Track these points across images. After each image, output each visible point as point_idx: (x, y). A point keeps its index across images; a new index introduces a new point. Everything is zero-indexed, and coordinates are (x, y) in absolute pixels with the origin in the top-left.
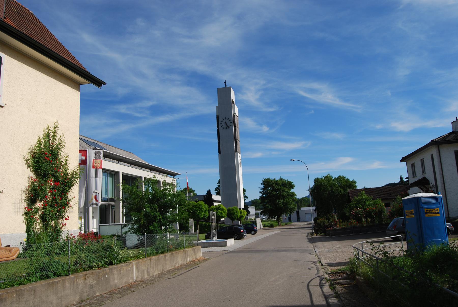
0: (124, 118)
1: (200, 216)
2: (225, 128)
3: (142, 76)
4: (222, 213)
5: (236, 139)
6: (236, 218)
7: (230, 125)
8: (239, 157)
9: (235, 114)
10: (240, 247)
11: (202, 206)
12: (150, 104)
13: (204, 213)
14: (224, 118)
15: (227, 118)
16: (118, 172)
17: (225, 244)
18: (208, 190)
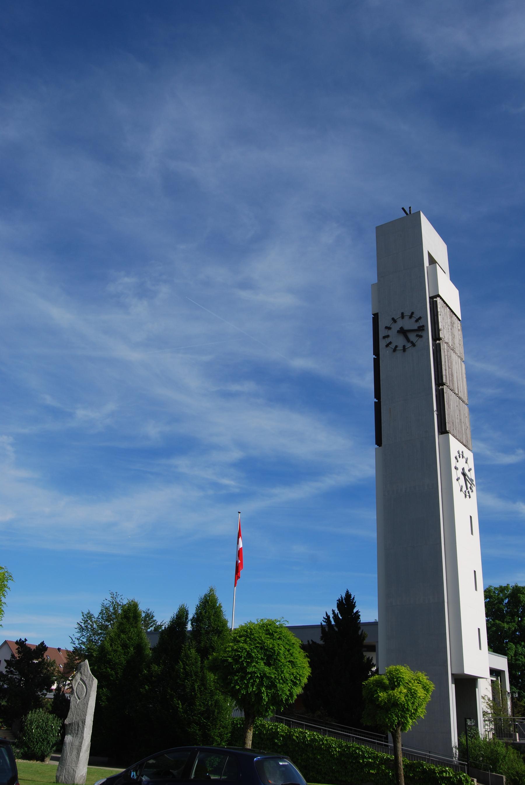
5: (443, 384)
8: (453, 454)
9: (439, 296)
15: (407, 313)
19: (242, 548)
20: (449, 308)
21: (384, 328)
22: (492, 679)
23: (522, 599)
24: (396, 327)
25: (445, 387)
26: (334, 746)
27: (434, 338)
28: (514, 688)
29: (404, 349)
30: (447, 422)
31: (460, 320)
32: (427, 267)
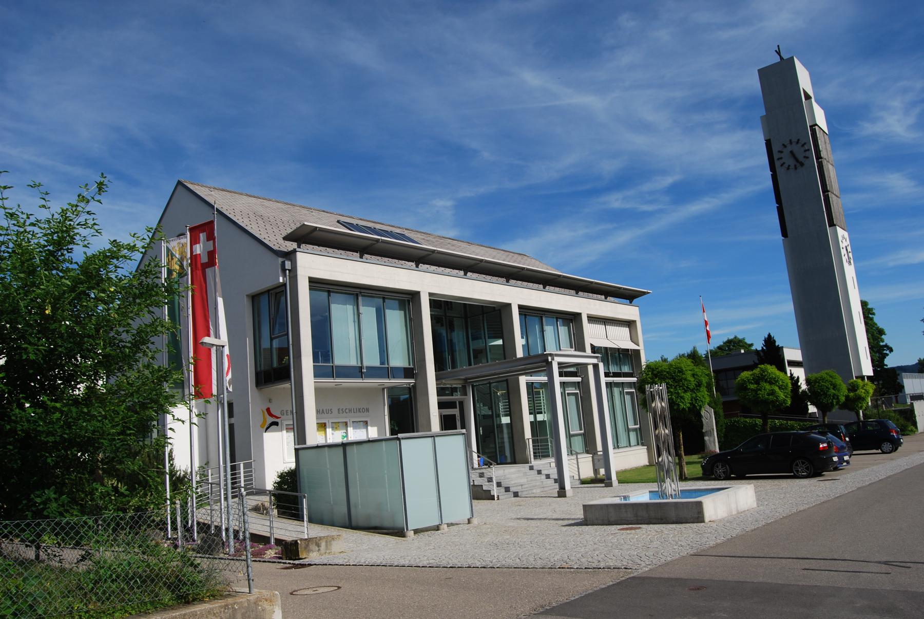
0: (620, 218)
1: (678, 405)
2: (792, 167)
3: (645, 127)
4: (772, 390)
5: (828, 191)
6: (832, 403)
7: (805, 157)
8: (840, 239)
9: (816, 125)
10: (717, 545)
11: (684, 374)
12: (669, 180)
13: (694, 395)
14: (787, 142)
15: (794, 140)
16: (508, 306)
17: (695, 514)
18: (766, 336)
25: (829, 193)
29: (796, 168)
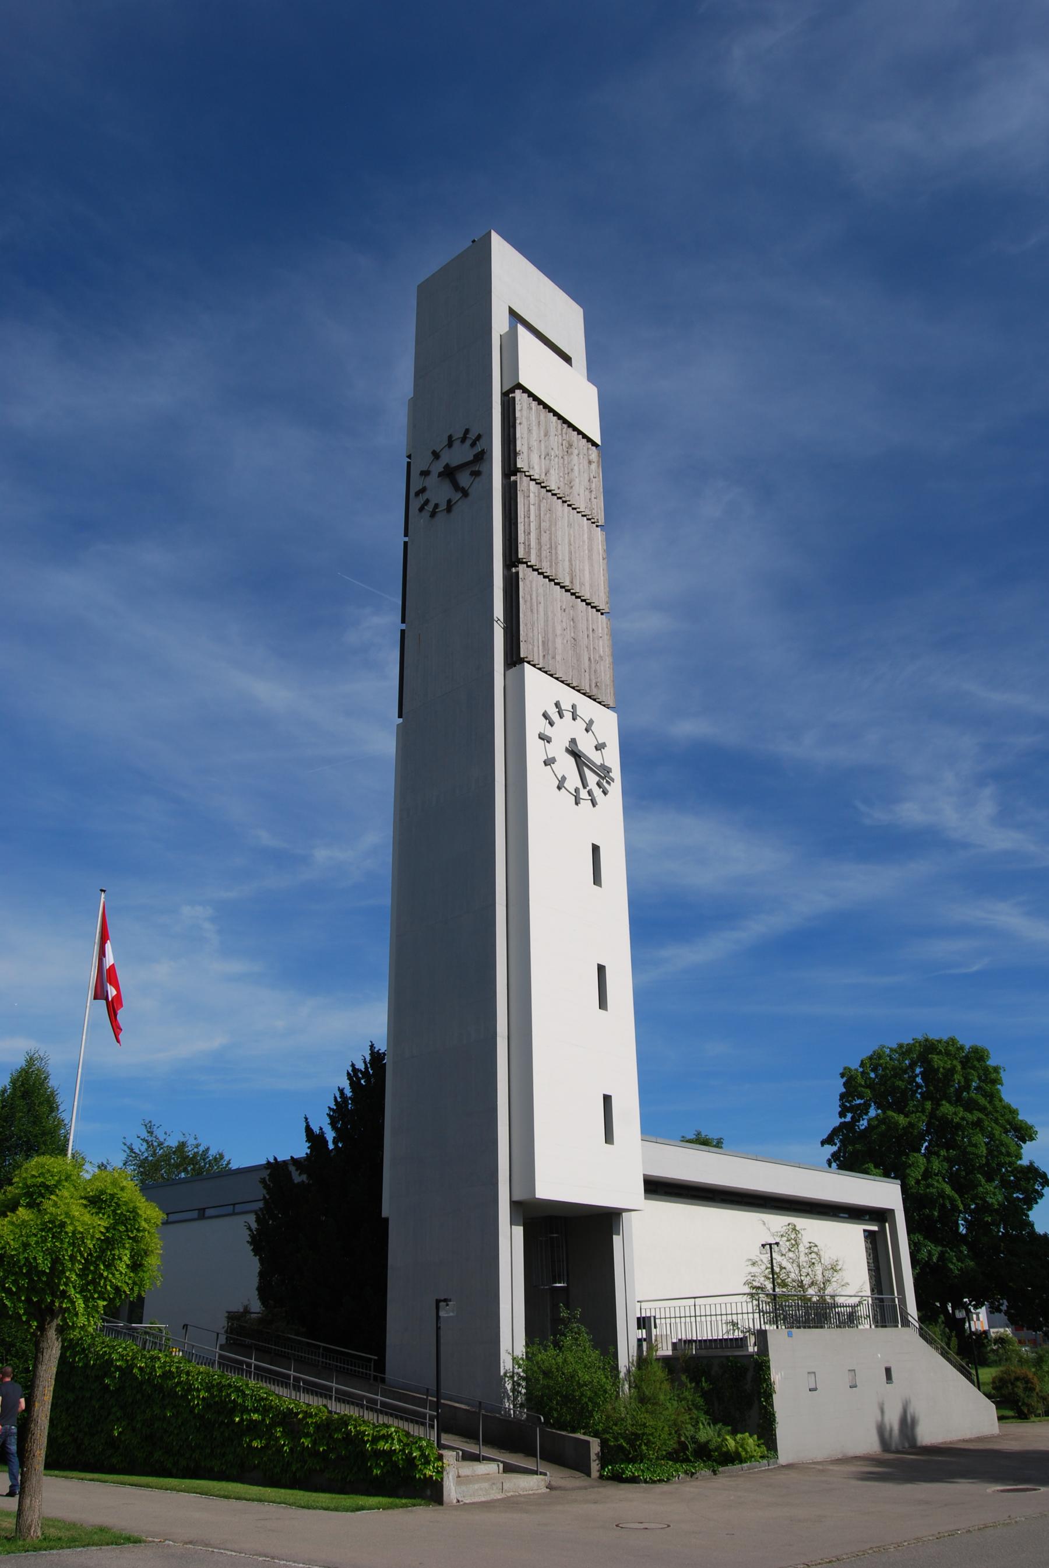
9: (519, 386)
19: (113, 964)
20: (556, 414)
21: (418, 474)
22: (865, 1228)
23: (936, 1063)
24: (438, 467)
25: (522, 568)
26: (196, 1386)
27: (506, 472)
28: (929, 1243)
29: (449, 508)
30: (521, 639)
31: (599, 445)
32: (501, 335)
